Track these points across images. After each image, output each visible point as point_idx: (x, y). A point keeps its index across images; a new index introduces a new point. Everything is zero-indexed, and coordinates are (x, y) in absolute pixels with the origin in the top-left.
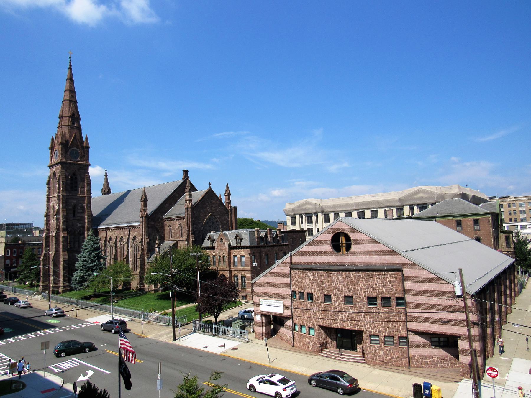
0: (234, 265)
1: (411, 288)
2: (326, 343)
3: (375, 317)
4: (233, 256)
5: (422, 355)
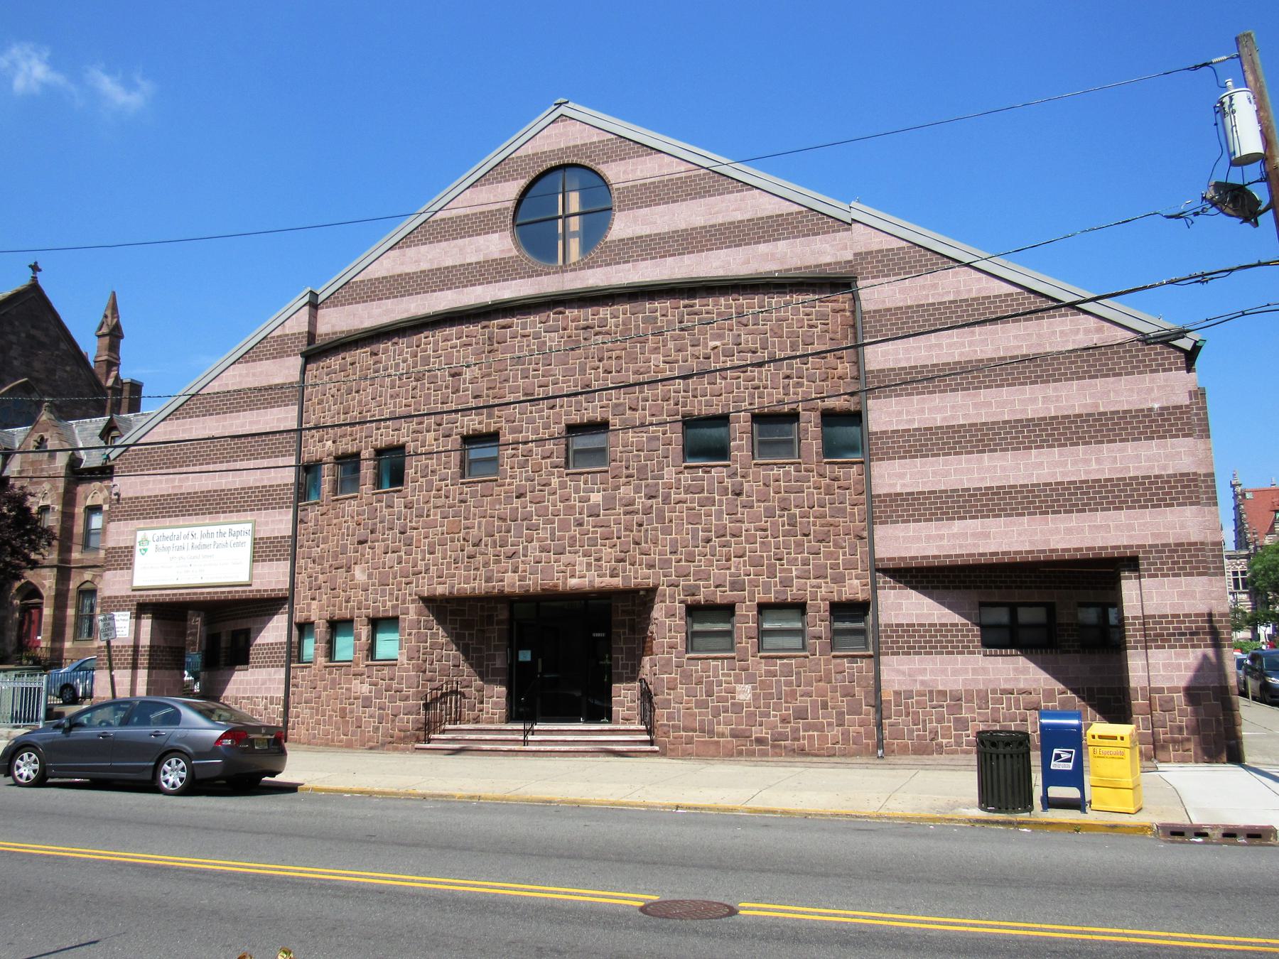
0: (86, 545)
1: (898, 360)
2: (456, 692)
3: (719, 515)
4: (82, 510)
5: (940, 688)
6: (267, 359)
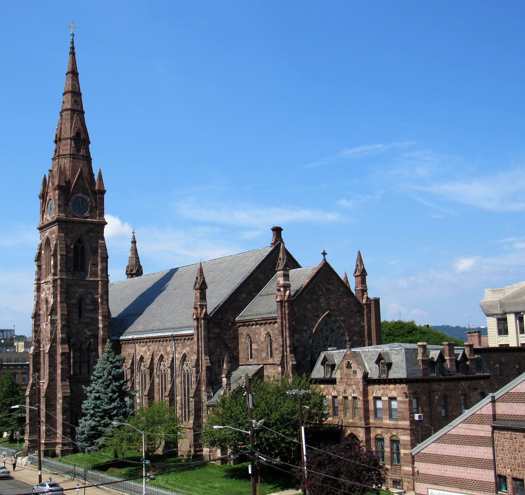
0: (376, 416)
4: (372, 397)
6: (476, 424)
